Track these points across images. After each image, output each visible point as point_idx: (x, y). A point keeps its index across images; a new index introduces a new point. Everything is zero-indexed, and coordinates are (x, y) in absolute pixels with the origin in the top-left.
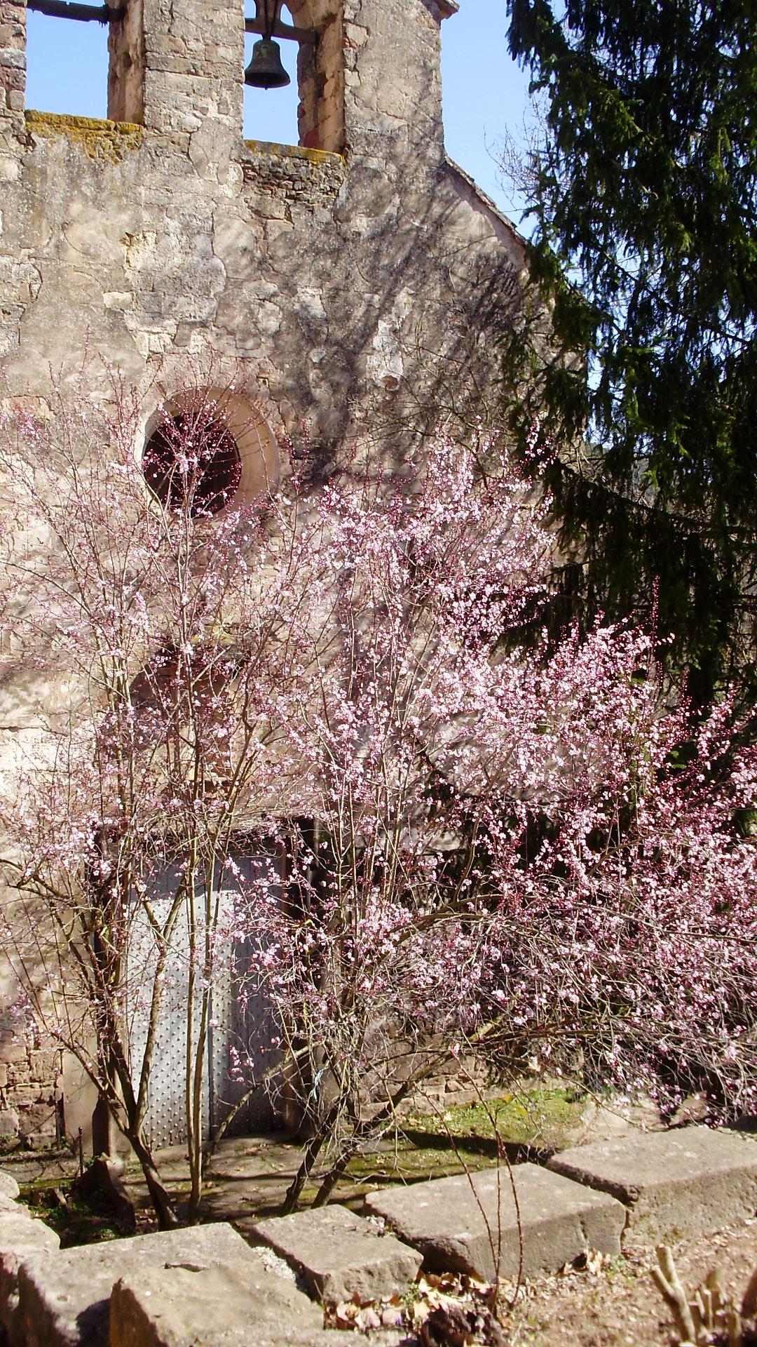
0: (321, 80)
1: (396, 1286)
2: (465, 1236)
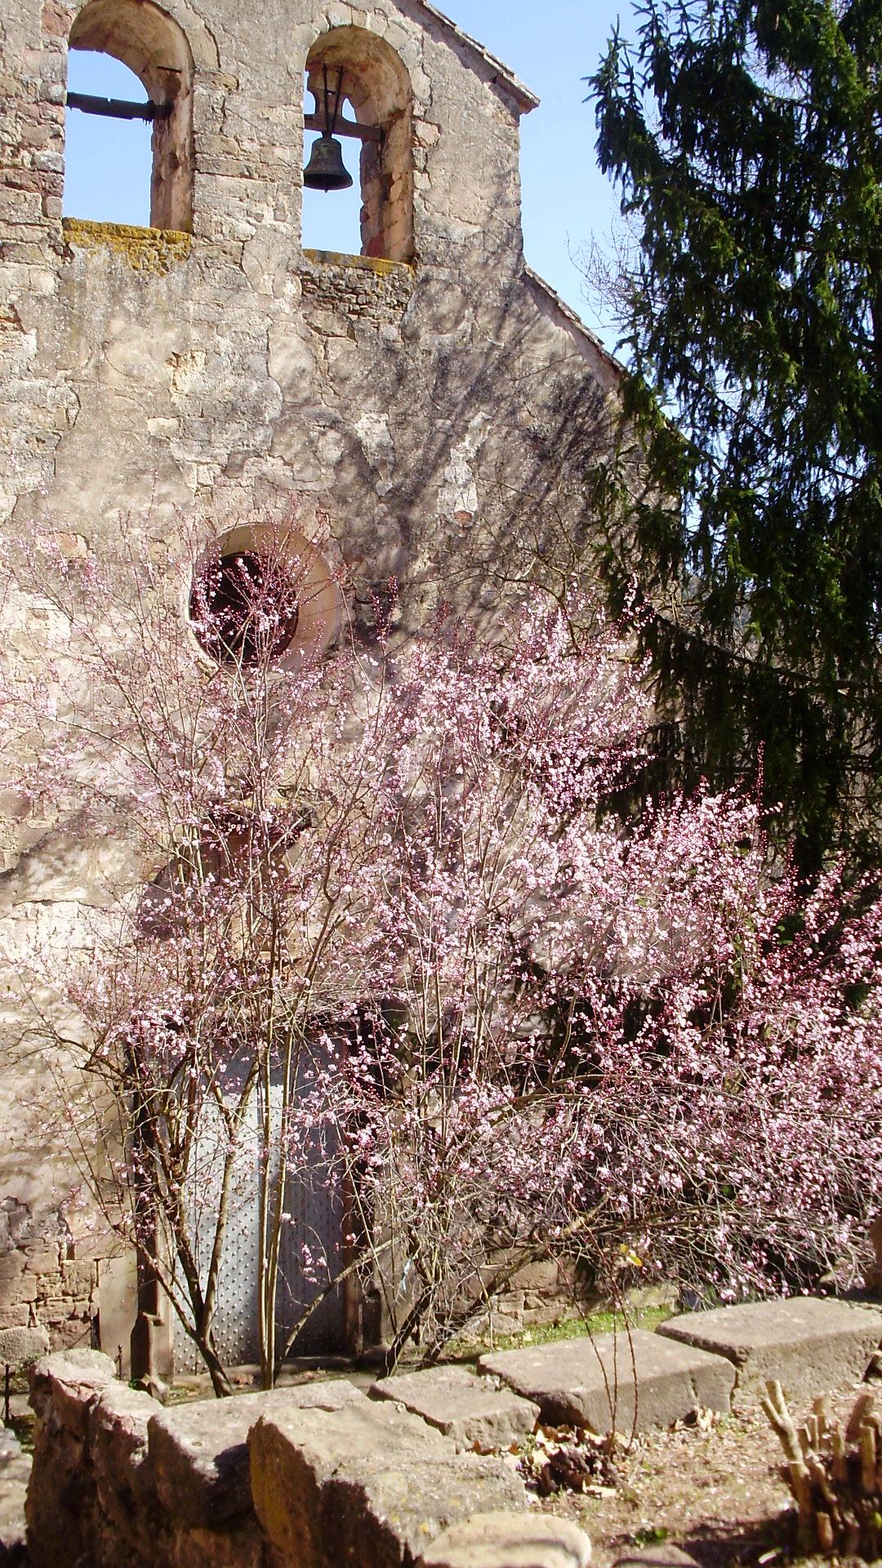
0: (387, 182)
1: (514, 1437)
2: (579, 1389)
